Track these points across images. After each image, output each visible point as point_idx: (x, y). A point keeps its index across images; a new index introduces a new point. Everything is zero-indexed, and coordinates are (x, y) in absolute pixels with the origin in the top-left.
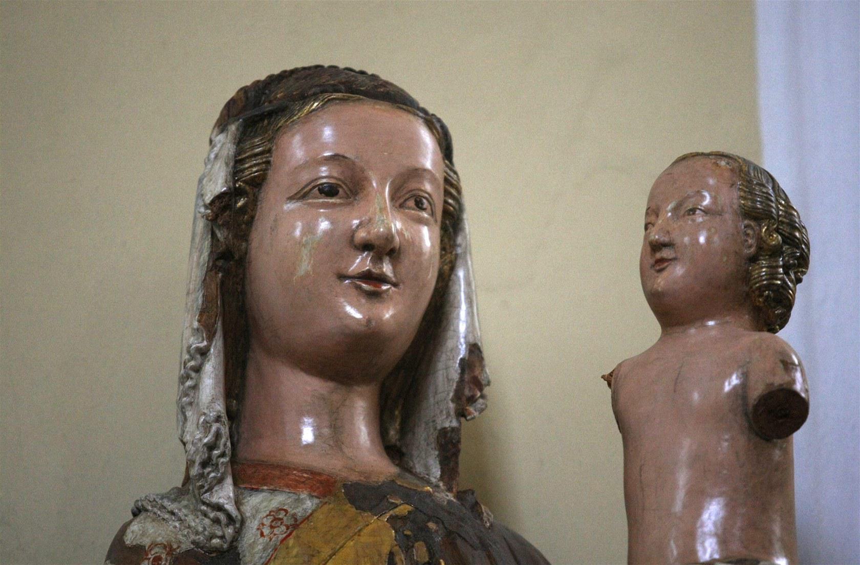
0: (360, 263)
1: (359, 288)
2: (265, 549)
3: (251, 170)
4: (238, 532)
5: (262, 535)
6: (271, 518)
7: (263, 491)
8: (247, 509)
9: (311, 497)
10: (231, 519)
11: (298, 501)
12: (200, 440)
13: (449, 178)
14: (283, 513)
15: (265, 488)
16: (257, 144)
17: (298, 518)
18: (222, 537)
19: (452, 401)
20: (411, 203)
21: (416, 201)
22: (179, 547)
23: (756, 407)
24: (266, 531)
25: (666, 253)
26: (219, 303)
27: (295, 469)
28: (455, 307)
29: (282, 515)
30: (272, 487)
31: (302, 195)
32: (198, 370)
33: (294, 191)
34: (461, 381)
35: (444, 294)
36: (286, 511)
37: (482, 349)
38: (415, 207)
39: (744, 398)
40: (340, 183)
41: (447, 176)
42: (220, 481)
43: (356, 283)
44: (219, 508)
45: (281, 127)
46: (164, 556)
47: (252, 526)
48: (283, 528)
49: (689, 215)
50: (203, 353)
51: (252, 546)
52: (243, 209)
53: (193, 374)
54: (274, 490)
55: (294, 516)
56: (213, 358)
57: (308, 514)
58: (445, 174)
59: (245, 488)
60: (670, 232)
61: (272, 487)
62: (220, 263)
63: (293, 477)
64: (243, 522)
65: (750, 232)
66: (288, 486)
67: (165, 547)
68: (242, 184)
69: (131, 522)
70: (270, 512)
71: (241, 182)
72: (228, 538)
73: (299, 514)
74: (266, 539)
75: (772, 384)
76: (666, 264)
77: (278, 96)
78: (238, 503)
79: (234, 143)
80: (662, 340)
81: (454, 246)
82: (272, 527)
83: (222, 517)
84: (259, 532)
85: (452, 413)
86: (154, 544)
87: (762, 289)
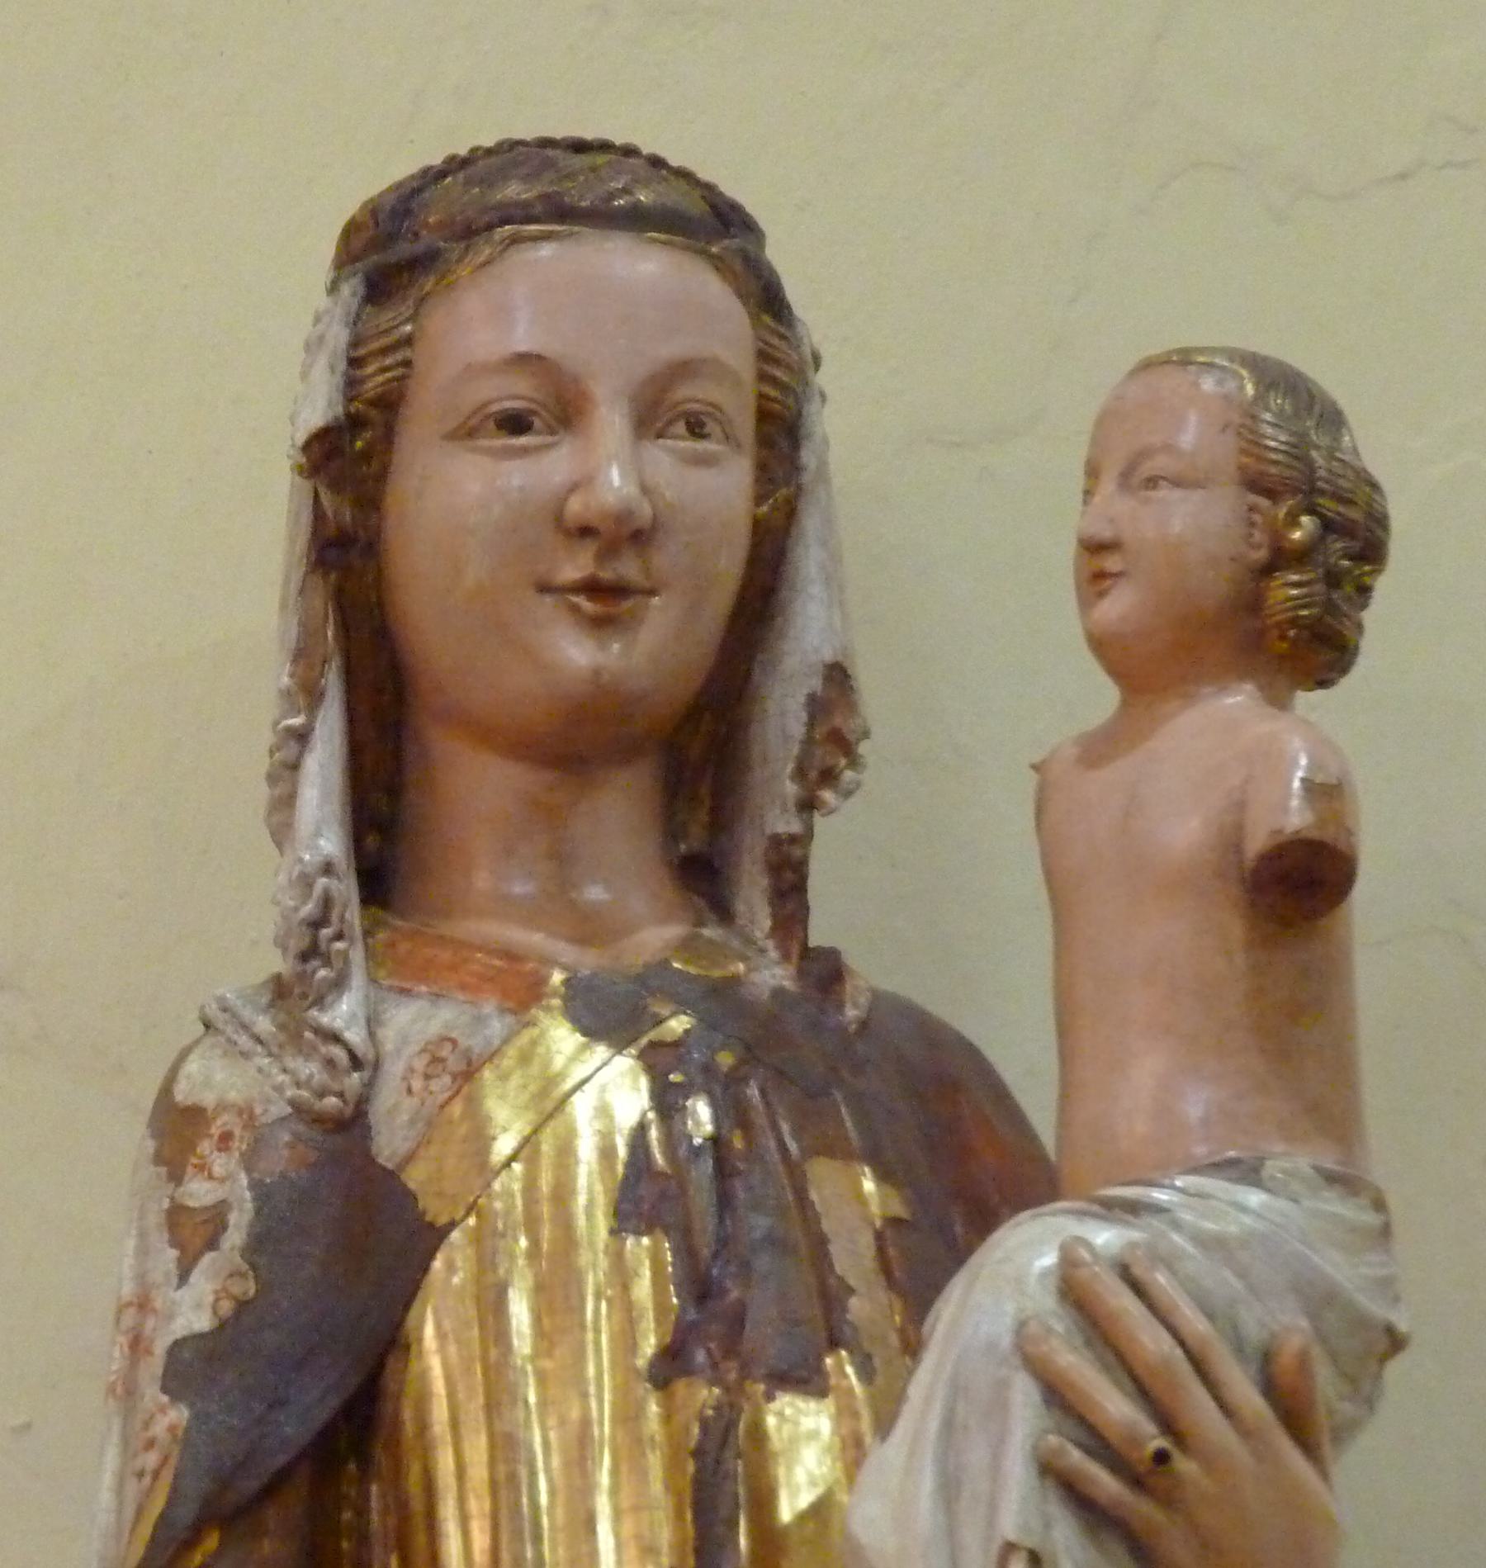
0: (575, 566)
1: (575, 609)
2: (412, 1122)
3: (374, 382)
4: (369, 1085)
5: (409, 1091)
6: (426, 1058)
7: (419, 996)
8: (389, 1036)
9: (503, 1011)
10: (356, 1062)
11: (480, 1020)
12: (296, 909)
13: (770, 350)
14: (448, 1046)
15: (424, 988)
16: (393, 318)
17: (474, 1057)
18: (340, 1095)
19: (792, 779)
20: (680, 428)
21: (688, 424)
22: (266, 1111)
23: (1256, 872)
24: (417, 1084)
25: (1112, 563)
26: (330, 634)
27: (480, 949)
28: (797, 591)
29: (446, 1051)
30: (435, 989)
31: (466, 433)
32: (294, 766)
33: (452, 424)
34: (808, 742)
35: (778, 567)
36: (454, 1042)
37: (850, 672)
38: (686, 434)
39: (1238, 848)
40: (533, 406)
41: (782, 330)
42: (339, 984)
43: (570, 600)
44: (335, 1038)
45: (428, 294)
46: (237, 1132)
47: (393, 1070)
48: (447, 1079)
49: (1147, 488)
50: (302, 737)
51: (394, 1110)
52: (366, 456)
53: (286, 774)
54: (437, 995)
55: (468, 1051)
56: (319, 746)
57: (493, 1050)
58: (761, 344)
59: (390, 988)
60: (1106, 533)
61: (435, 989)
62: (332, 554)
63: (475, 967)
64: (377, 1065)
65: (1257, 518)
66: (463, 987)
67: (240, 1113)
68: (360, 406)
69: (197, 1042)
70: (426, 1044)
71: (361, 402)
72: (351, 1096)
73: (477, 1051)
74: (415, 1100)
75: (1280, 832)
76: (1108, 582)
77: (430, 220)
78: (373, 1023)
79: (347, 324)
80: (1125, 704)
81: (794, 467)
82: (427, 1077)
83: (338, 1053)
84: (404, 1085)
85: (791, 804)
86: (222, 1107)
87: (1285, 626)
